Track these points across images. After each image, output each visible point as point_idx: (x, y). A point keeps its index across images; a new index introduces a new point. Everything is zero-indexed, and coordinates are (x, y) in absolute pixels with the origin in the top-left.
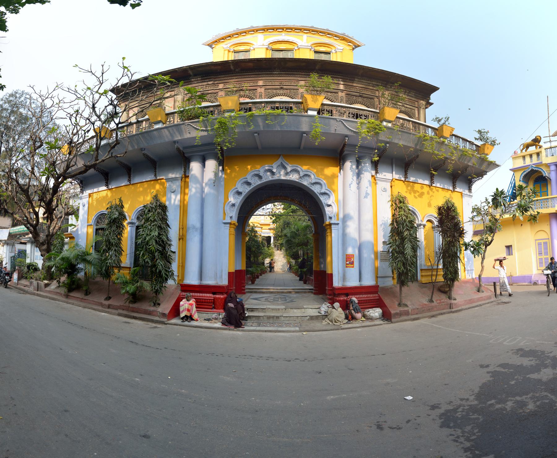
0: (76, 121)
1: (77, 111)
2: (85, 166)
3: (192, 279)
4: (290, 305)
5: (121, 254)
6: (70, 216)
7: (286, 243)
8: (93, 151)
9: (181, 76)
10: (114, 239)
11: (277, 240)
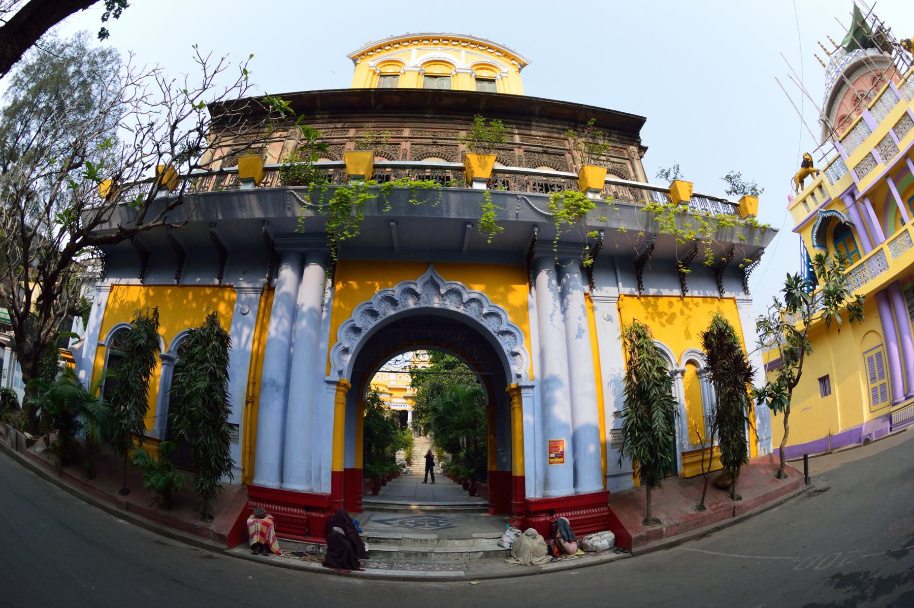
0: (142, 142)
1: (152, 125)
2: (120, 228)
3: (267, 479)
5: (144, 412)
6: (76, 317)
8: (141, 206)
9: (309, 107)
10: (136, 382)
11: (420, 418)
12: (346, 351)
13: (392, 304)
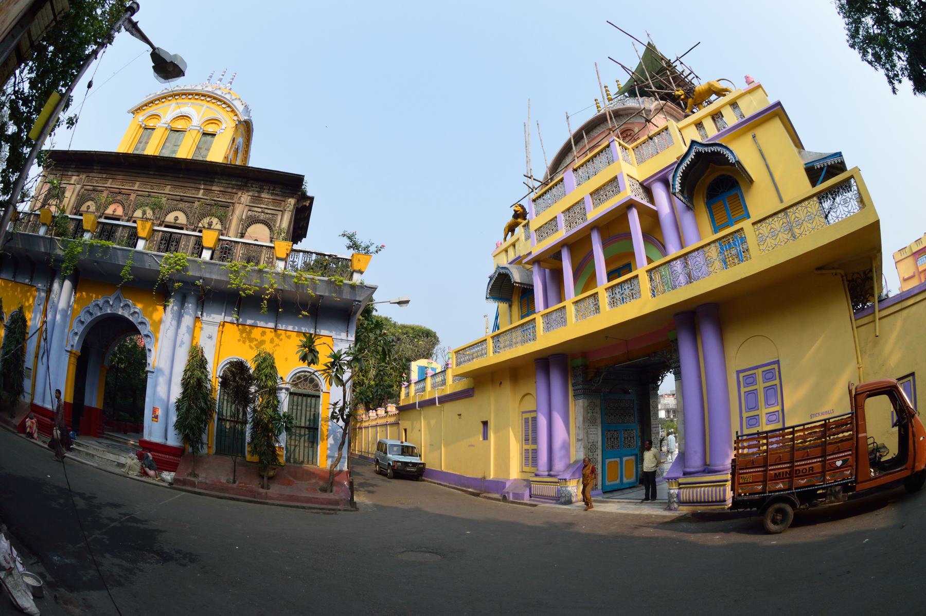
12: (76, 334)
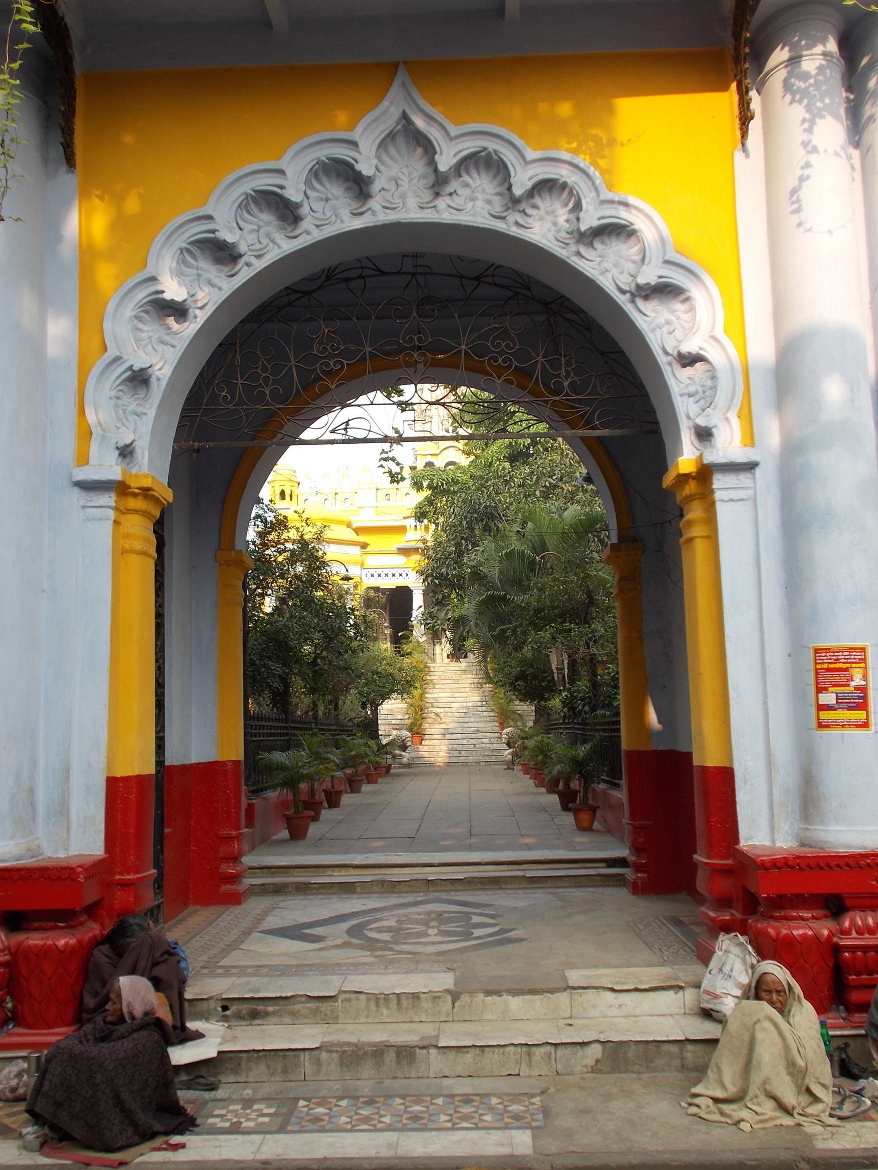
4: (487, 965)
7: (480, 613)
13: (282, 218)
